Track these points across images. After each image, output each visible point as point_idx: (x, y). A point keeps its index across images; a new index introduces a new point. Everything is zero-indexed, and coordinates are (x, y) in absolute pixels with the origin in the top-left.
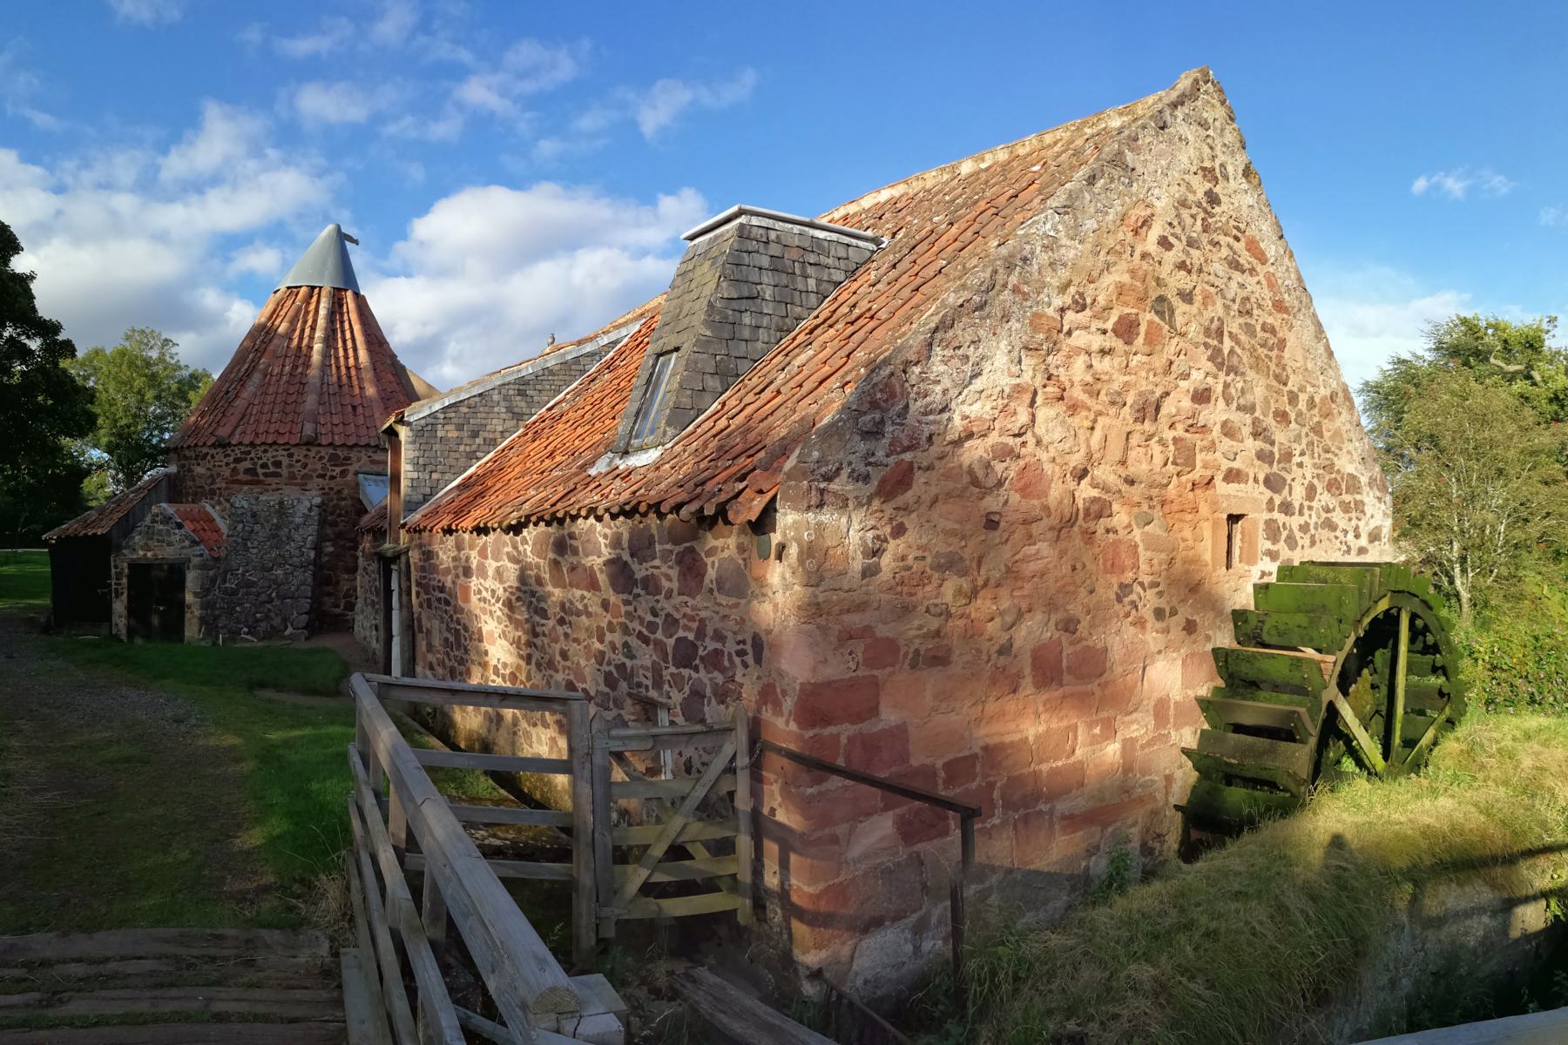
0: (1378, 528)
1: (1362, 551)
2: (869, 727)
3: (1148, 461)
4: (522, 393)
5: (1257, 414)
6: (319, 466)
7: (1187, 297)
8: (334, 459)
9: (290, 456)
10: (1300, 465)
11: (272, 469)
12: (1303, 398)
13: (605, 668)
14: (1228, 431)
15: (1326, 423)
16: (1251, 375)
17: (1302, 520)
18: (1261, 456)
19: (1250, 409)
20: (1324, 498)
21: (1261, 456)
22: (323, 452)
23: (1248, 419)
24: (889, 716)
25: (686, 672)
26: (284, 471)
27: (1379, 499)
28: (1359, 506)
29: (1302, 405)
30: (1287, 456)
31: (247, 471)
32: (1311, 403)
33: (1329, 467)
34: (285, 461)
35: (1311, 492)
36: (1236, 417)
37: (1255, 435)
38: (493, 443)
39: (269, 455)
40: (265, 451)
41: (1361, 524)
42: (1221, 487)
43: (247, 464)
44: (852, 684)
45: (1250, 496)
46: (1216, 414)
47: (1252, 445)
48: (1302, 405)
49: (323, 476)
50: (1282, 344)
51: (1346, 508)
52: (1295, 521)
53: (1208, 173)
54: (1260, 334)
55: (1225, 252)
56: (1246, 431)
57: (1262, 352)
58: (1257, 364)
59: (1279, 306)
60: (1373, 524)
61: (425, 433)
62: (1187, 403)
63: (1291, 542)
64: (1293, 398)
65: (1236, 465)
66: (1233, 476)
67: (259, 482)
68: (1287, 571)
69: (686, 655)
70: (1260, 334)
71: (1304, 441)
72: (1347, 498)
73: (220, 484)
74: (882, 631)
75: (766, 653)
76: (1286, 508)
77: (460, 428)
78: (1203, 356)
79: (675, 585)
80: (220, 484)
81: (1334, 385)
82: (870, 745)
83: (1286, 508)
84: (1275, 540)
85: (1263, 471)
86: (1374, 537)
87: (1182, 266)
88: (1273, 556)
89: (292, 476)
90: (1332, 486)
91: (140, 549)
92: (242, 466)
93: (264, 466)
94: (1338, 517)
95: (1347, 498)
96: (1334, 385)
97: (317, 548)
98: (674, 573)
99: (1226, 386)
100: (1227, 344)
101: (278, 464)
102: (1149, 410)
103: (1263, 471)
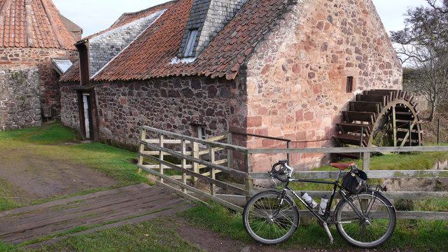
0: (398, 80)
1: (391, 87)
2: (260, 128)
3: (339, 94)
5: (357, 46)
6: (35, 56)
9: (23, 52)
10: (370, 60)
11: (15, 57)
12: (372, 40)
13: (182, 118)
14: (348, 51)
16: (355, 34)
17: (370, 78)
18: (357, 58)
19: (354, 45)
20: (379, 71)
21: (357, 58)
22: (37, 50)
24: (263, 126)
25: (210, 117)
26: (21, 58)
27: (398, 70)
28: (391, 73)
29: (371, 42)
30: (366, 58)
32: (375, 41)
33: (380, 60)
34: (21, 54)
35: (374, 69)
36: (349, 47)
39: (13, 51)
40: (11, 50)
41: (391, 78)
42: (345, 69)
44: (256, 118)
45: (354, 72)
47: (354, 55)
48: (371, 42)
49: (38, 60)
51: (386, 73)
54: (358, 21)
56: (353, 51)
57: (358, 27)
58: (358, 31)
59: (364, 12)
60: (396, 78)
63: (367, 84)
65: (349, 61)
66: (349, 65)
67: (9, 63)
68: (364, 92)
69: (210, 113)
70: (358, 21)
71: (372, 53)
72: (387, 70)
74: (262, 106)
75: (235, 111)
76: (366, 74)
79: (207, 95)
81: (383, 34)
82: (260, 131)
83: (366, 74)
85: (358, 63)
86: (396, 82)
88: (361, 89)
89: (24, 60)
90: (382, 67)
94: (383, 76)
95: (387, 70)
96: (383, 34)
98: (207, 92)
100: (348, 26)
101: (17, 55)
103: (358, 63)
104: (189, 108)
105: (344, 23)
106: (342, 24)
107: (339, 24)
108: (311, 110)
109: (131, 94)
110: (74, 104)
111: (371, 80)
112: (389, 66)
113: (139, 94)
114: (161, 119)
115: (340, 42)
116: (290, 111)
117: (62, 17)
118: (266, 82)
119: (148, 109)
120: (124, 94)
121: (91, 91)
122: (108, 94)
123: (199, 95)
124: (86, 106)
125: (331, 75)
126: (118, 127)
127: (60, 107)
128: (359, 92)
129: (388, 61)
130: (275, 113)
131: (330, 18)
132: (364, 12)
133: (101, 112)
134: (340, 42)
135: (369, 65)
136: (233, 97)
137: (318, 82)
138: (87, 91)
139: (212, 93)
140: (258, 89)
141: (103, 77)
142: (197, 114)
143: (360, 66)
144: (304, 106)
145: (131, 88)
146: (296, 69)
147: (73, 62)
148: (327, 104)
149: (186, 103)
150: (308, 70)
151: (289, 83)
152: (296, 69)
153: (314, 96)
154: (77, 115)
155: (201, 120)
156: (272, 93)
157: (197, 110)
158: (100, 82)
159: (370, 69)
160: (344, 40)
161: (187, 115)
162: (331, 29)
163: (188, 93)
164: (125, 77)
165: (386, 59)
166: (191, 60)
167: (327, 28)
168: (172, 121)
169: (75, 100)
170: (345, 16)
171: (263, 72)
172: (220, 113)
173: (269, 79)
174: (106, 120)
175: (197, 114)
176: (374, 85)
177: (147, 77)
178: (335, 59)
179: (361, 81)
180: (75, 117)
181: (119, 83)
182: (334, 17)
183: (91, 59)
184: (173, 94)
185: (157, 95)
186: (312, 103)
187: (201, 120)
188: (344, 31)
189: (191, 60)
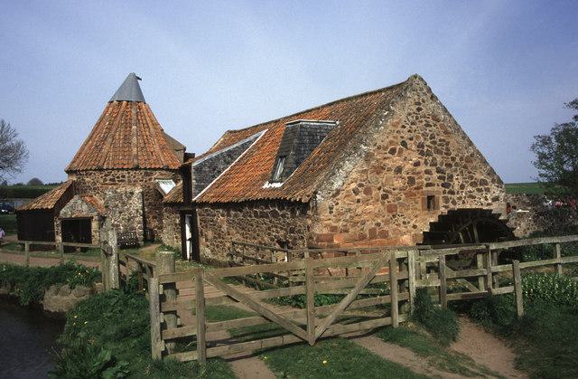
1: (489, 204)
4: (229, 156)
7: (411, 139)
8: (147, 174)
14: (427, 172)
15: (468, 165)
18: (439, 178)
19: (435, 165)
23: (434, 168)
28: (488, 190)
30: (451, 177)
31: (111, 180)
32: (461, 159)
34: (127, 175)
35: (462, 187)
37: (438, 172)
38: (220, 172)
42: (425, 189)
43: (111, 177)
45: (437, 189)
46: (422, 168)
50: (448, 144)
51: (479, 190)
52: (455, 197)
53: (416, 104)
55: (424, 123)
58: (438, 152)
59: (446, 132)
61: (199, 169)
62: (411, 167)
63: (454, 203)
64: (453, 159)
69: (292, 231)
73: (98, 185)
74: (334, 224)
77: (209, 167)
78: (417, 154)
80: (98, 185)
84: (447, 202)
87: (409, 131)
88: (446, 207)
89: (130, 181)
91: (66, 212)
92: (108, 178)
93: (118, 177)
97: (143, 209)
99: (426, 160)
100: (426, 148)
101: (123, 176)
102: (399, 170)
104: (276, 227)
105: (421, 146)
106: (418, 147)
107: (414, 147)
108: (386, 228)
109: (229, 215)
110: (176, 225)
111: (460, 198)
112: (484, 182)
113: (236, 216)
114: (255, 238)
115: (417, 164)
116: (362, 229)
117: (167, 137)
118: (337, 204)
119: (243, 229)
120: (223, 215)
121: (193, 213)
122: (208, 215)
123: (284, 216)
124: (188, 235)
125: (409, 195)
126: (218, 246)
127: (161, 228)
128: (443, 211)
129: (482, 177)
130: (347, 231)
131: (404, 144)
132: (446, 132)
133: (201, 232)
134: (417, 164)
135: (456, 185)
136: (309, 217)
137: (392, 203)
138: (189, 212)
139: (293, 212)
140: (328, 211)
141: (204, 200)
142: (282, 233)
143: (443, 185)
144: (378, 224)
145: (228, 211)
146: (368, 191)
147: (176, 182)
148: (404, 223)
149: (274, 223)
150: (382, 192)
151: (360, 204)
152: (368, 191)
153: (388, 216)
154: (179, 236)
155: (286, 238)
156: (343, 214)
157: (282, 229)
158: (202, 205)
159: (456, 188)
160: (422, 161)
161: (274, 234)
162: (405, 153)
163: (275, 214)
164: (224, 200)
165: (479, 176)
166: (278, 185)
167: (401, 152)
168: (263, 239)
169: (178, 221)
170: (422, 139)
171: (334, 196)
172: (299, 231)
173: (339, 202)
174: (207, 240)
175: (282, 233)
176: (464, 202)
177: (243, 199)
178: (411, 181)
179: (446, 200)
180: (176, 238)
181: (217, 205)
182: (408, 142)
183: (194, 181)
184: (263, 215)
185: (250, 216)
186: (387, 222)
187: (286, 238)
188: (422, 153)
189: (278, 185)
